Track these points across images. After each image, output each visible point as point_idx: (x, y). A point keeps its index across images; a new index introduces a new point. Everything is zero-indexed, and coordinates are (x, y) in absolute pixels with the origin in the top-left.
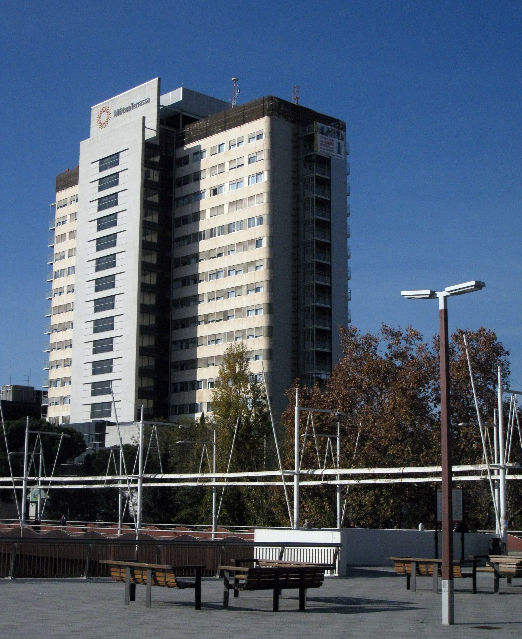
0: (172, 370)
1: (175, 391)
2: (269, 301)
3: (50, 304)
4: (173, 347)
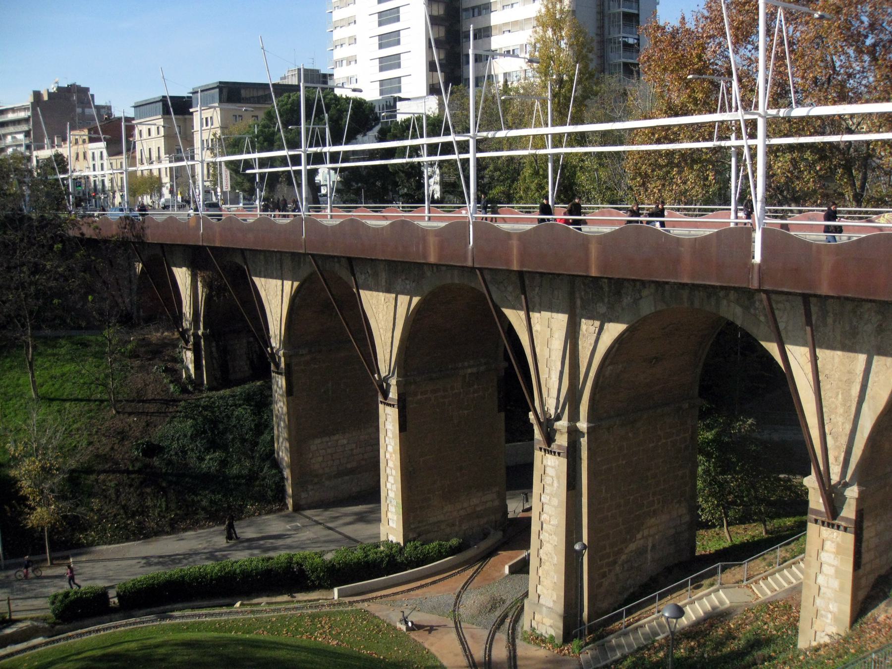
0: (464, 40)
3: (331, 18)
4: (464, 15)
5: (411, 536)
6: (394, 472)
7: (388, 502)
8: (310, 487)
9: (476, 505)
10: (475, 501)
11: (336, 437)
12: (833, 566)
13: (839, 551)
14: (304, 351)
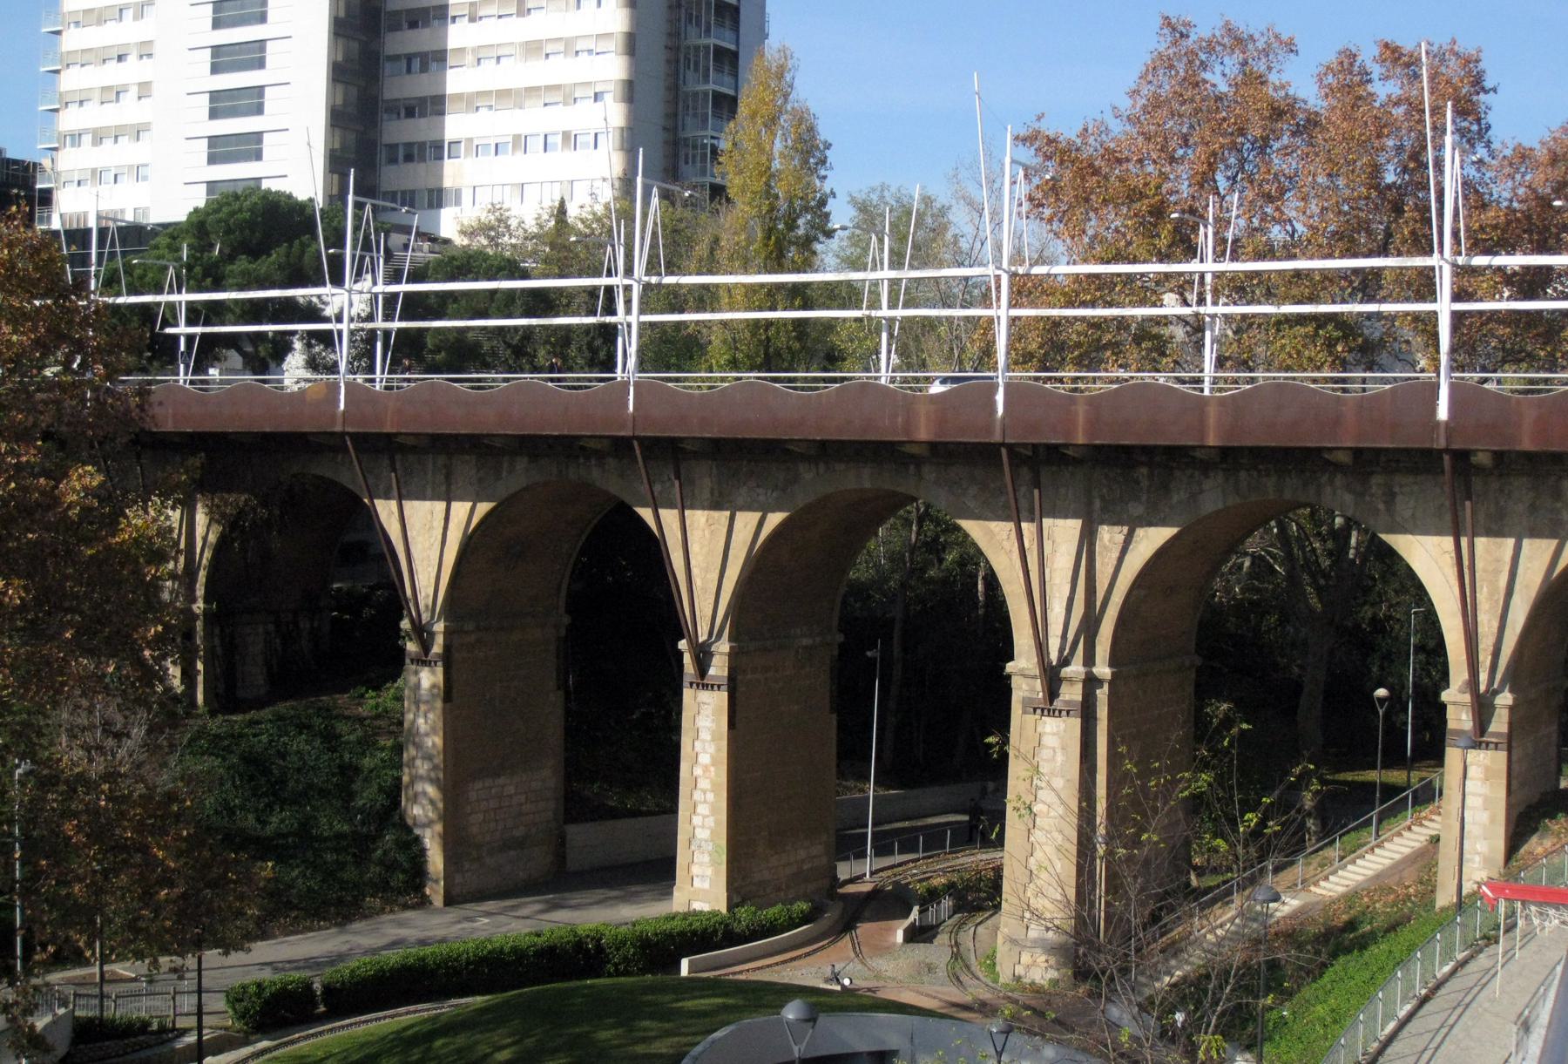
0: (385, 116)
1: (393, 160)
2: (630, 73)
4: (388, 67)
5: (736, 900)
6: (710, 797)
7: (693, 848)
8: (467, 866)
9: (803, 861)
10: (802, 854)
11: (501, 781)
12: (1480, 795)
13: (1488, 775)
14: (470, 626)
